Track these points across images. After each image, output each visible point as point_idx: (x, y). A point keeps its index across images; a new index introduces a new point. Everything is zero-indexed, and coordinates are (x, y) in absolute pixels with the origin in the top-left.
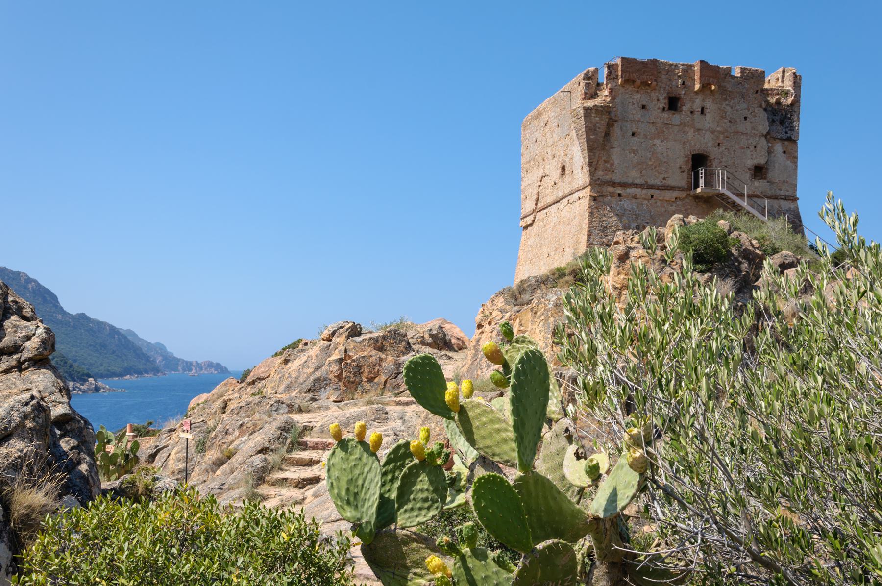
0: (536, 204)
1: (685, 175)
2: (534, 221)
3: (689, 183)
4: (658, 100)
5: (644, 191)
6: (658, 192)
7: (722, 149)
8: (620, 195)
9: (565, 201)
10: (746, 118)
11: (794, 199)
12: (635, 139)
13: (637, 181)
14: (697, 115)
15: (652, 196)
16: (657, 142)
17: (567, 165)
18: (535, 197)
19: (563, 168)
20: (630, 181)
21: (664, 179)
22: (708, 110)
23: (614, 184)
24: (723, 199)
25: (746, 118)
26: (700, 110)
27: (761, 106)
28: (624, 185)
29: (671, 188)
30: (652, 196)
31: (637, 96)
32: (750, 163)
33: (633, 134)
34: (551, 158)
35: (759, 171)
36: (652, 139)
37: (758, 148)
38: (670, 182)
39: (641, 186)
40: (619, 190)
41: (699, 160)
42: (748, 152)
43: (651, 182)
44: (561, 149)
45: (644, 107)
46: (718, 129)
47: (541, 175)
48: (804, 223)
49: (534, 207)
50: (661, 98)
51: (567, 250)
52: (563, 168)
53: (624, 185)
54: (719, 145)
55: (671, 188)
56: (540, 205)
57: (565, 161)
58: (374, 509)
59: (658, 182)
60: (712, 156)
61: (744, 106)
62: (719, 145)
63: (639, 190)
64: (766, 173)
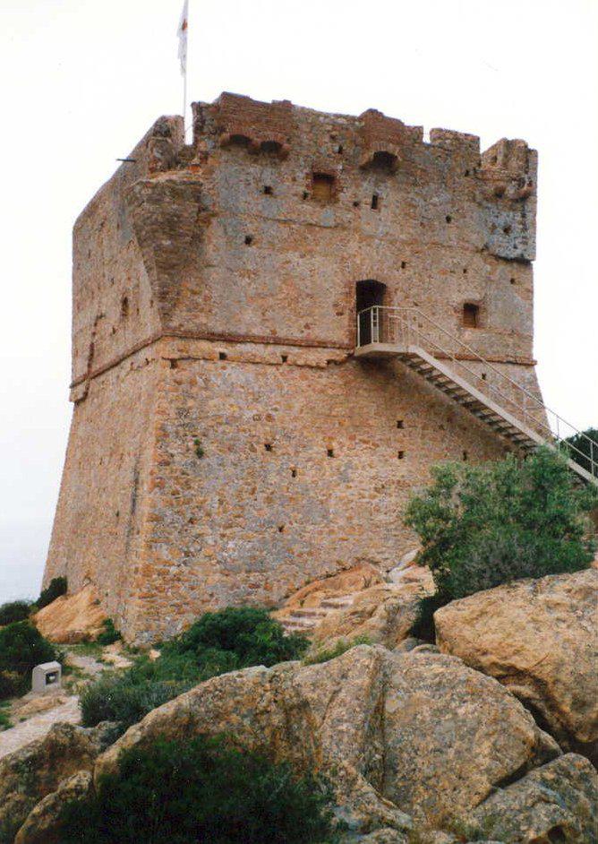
0: (89, 366)
1: (345, 320)
2: (86, 394)
3: (352, 335)
4: (294, 180)
5: (270, 348)
6: (296, 350)
7: (409, 272)
8: (223, 356)
9: (127, 364)
10: (448, 219)
11: (530, 364)
12: (252, 249)
13: (256, 331)
14: (366, 208)
15: (285, 358)
16: (294, 257)
17: (130, 298)
18: (87, 353)
19: (125, 302)
20: (242, 330)
21: (307, 326)
22: (384, 203)
23: (212, 337)
24: (412, 366)
25: (448, 219)
26: (370, 200)
27: (474, 200)
28: (230, 339)
29: (322, 345)
30: (285, 358)
31: (254, 169)
32: (458, 298)
33: (248, 241)
34: (108, 284)
35: (471, 313)
36: (282, 250)
37: (470, 273)
38: (318, 333)
39: (264, 341)
40: (220, 348)
41: (369, 294)
42: (454, 279)
43: (282, 333)
44: (122, 268)
45: (268, 191)
46: (403, 237)
47: (95, 314)
48: (546, 404)
49: (86, 369)
50: (300, 175)
51: (127, 459)
52: (125, 302)
53: (230, 339)
54: (403, 265)
55: (322, 345)
56: (96, 367)
57: (127, 291)
58: (52, 604)
59: (297, 335)
60: (390, 284)
61: (446, 196)
62: (403, 265)
63: (260, 347)
64: (481, 316)
